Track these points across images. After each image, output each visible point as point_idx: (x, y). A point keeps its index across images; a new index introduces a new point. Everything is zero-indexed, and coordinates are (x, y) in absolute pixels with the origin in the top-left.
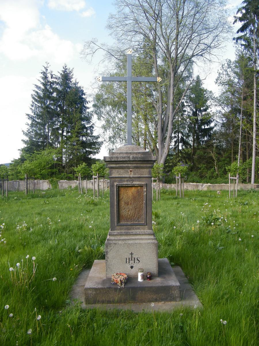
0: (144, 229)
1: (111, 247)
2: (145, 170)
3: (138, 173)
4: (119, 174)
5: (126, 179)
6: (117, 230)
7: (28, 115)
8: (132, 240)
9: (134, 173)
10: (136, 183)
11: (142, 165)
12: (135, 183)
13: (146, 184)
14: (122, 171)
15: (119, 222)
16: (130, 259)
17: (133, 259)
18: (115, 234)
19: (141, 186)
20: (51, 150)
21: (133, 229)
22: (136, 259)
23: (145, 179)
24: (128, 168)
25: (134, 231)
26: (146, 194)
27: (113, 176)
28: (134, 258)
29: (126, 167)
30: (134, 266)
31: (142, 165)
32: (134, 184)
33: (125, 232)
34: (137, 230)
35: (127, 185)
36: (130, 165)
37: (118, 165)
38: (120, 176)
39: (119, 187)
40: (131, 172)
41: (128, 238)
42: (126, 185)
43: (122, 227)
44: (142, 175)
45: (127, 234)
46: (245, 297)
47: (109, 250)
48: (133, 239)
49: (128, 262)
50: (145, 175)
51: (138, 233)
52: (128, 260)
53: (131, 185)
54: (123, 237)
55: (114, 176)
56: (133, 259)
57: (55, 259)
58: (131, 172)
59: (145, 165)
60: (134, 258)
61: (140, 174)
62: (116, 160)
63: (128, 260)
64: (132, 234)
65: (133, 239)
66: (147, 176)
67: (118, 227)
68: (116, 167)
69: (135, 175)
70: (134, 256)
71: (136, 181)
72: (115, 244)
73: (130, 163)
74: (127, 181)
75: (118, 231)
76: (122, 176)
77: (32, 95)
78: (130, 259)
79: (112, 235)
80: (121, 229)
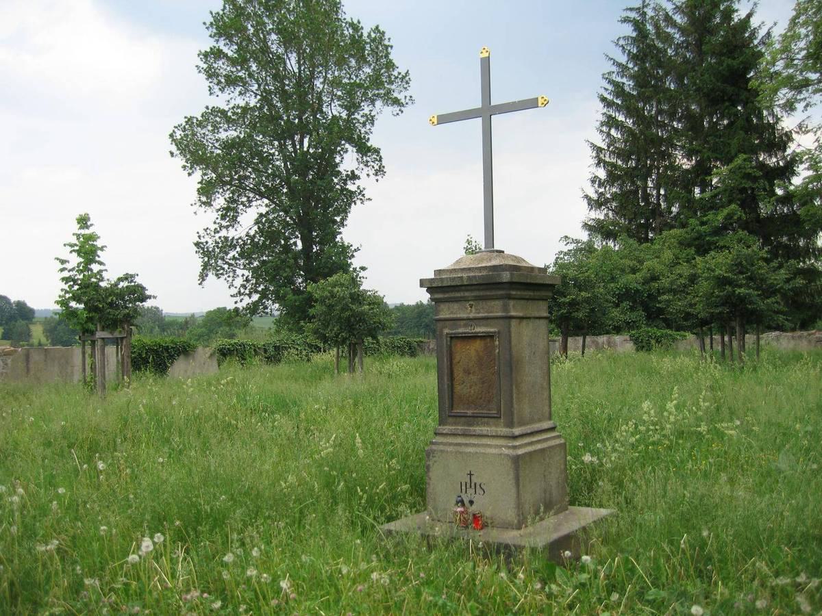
0: (496, 426)
1: (435, 457)
2: (497, 302)
3: (483, 308)
4: (452, 313)
5: (462, 323)
6: (450, 424)
7: (586, 196)
8: (472, 447)
9: (476, 310)
10: (480, 329)
11: (488, 293)
12: (478, 329)
13: (499, 332)
14: (456, 306)
15: (452, 410)
16: (468, 486)
17: (473, 485)
18: (444, 432)
19: (490, 336)
20: (787, 287)
21: (478, 425)
22: (478, 487)
23: (496, 321)
24: (465, 299)
25: (478, 429)
26: (499, 353)
27: (442, 316)
28: (475, 484)
29: (461, 297)
30: (474, 500)
31: (488, 293)
32: (475, 333)
33: (462, 429)
34: (484, 426)
35: (465, 333)
36: (467, 294)
37: (447, 296)
38: (452, 316)
39: (451, 338)
40: (471, 307)
41: (468, 442)
42: (462, 333)
43: (458, 419)
44: (491, 312)
45: (465, 435)
46: (645, 582)
47: (431, 463)
48: (474, 445)
49: (464, 491)
50: (497, 312)
51: (485, 433)
52: (464, 488)
53: (472, 335)
54: (460, 440)
55: (442, 317)
56: (473, 485)
57: (679, 598)
58: (471, 307)
59: (493, 293)
60: (475, 484)
61: (486, 312)
62: (440, 285)
63: (464, 488)
64: (474, 433)
65: (474, 445)
66: (500, 314)
67: (450, 420)
68: (444, 298)
69: (479, 313)
70: (474, 479)
71: (480, 326)
72: (442, 451)
73: (467, 290)
74: (465, 326)
75: (451, 428)
76: (455, 316)
77: (380, 171)
78: (468, 486)
79: (439, 434)
80: (456, 424)
